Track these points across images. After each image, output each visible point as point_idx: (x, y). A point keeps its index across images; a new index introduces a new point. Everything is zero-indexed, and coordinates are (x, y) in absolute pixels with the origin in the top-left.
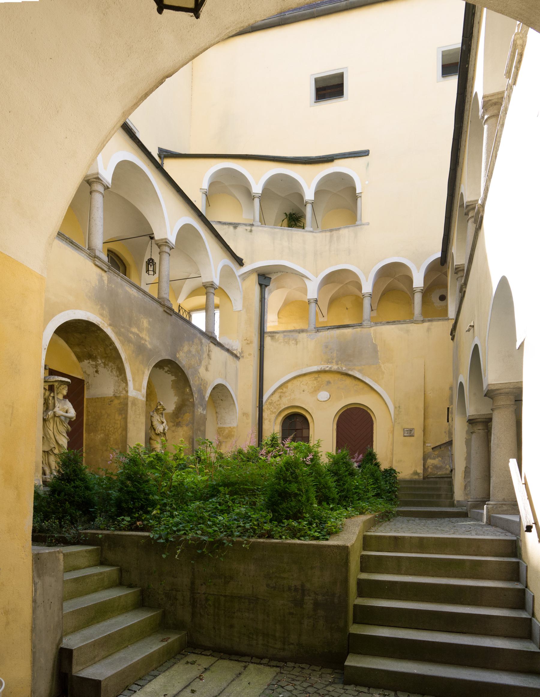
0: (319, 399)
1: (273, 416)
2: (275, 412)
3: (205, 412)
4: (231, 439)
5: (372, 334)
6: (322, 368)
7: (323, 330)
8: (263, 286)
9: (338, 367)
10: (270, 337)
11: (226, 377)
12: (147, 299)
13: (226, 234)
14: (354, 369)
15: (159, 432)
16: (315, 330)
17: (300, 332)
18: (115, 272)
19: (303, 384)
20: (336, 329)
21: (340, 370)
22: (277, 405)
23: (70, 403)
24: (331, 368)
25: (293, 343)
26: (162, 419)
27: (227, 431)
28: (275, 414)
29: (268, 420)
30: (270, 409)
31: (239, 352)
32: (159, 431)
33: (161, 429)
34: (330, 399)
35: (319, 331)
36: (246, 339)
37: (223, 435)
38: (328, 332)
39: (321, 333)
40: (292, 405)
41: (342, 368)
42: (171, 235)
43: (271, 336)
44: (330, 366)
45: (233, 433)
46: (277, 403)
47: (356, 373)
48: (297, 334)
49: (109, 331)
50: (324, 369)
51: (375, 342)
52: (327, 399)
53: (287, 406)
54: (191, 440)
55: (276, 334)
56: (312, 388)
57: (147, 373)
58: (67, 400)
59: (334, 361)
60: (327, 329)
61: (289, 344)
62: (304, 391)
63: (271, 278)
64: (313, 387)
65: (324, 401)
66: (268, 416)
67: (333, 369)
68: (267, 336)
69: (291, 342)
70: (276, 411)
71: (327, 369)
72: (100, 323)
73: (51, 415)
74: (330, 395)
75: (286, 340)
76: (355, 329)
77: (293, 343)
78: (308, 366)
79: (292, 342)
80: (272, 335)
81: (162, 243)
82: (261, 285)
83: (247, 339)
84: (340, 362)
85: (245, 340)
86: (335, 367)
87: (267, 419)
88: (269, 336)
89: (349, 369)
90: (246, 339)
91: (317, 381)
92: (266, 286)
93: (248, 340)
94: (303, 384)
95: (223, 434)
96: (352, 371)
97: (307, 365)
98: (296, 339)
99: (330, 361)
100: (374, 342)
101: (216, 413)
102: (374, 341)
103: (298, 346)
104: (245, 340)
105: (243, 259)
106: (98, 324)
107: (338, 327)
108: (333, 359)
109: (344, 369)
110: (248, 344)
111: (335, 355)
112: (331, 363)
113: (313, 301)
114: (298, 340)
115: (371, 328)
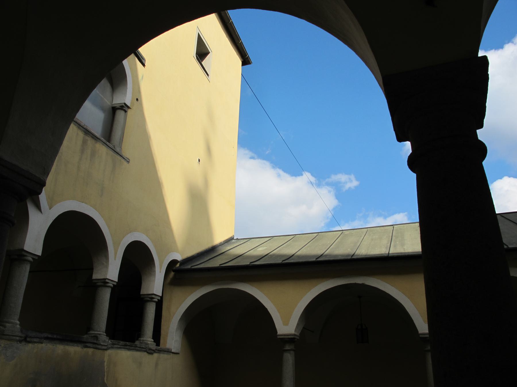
5: (105, 364)
16: (20, 334)
35: (28, 339)
38: (43, 345)
39: (30, 345)
51: (107, 380)
76: (85, 349)
100: (105, 381)
102: (105, 378)
115: (105, 351)
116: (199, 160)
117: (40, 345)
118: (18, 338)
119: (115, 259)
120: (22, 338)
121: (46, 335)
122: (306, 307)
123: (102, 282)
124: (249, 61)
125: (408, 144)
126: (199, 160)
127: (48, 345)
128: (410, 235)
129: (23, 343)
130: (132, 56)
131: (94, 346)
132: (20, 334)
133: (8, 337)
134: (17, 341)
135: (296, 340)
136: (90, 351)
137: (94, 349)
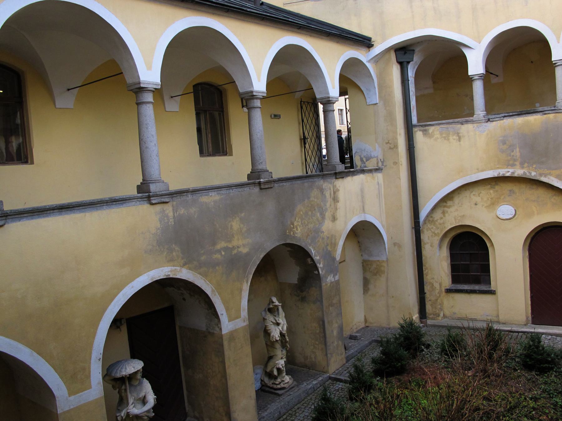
0: (499, 216)
1: (436, 240)
2: (438, 233)
3: (337, 278)
4: (381, 276)
6: (500, 173)
7: (496, 119)
8: (405, 64)
9: (524, 172)
10: (421, 132)
11: (363, 207)
12: (234, 192)
13: (344, 9)
14: (550, 174)
15: (274, 340)
16: (484, 119)
17: (464, 123)
18: (181, 193)
19: (474, 195)
20: (516, 116)
21: (528, 175)
22: (440, 224)
23: (149, 384)
24: (513, 173)
25: (454, 139)
26: (277, 319)
27: (374, 266)
28: (438, 236)
29: (429, 244)
30: (430, 230)
31: (381, 160)
32: (274, 338)
33: (277, 336)
34: (516, 216)
35: (491, 120)
36: (388, 143)
37: (371, 270)
38: (504, 120)
39: (494, 122)
40: (460, 224)
41: (530, 173)
42: (259, 81)
43: (423, 131)
44: (511, 170)
45: (382, 269)
46: (439, 221)
47: (553, 181)
48: (459, 126)
49: (185, 274)
50: (504, 174)
52: (511, 216)
53: (454, 226)
54: (321, 323)
55: (429, 127)
56: (488, 199)
57: (246, 287)
58: (145, 379)
59: (517, 163)
60: (502, 117)
61: (448, 140)
62: (476, 204)
63: (414, 50)
64: (490, 199)
65: (507, 219)
66: (429, 239)
67: (516, 175)
68: (417, 131)
69: (451, 138)
70: (439, 232)
71: (508, 175)
72: (169, 273)
73: (124, 416)
74: (515, 211)
75: (444, 135)
76: (545, 116)
77: (454, 139)
78: (479, 170)
79: (454, 137)
80: (424, 128)
81: (248, 97)
82: (401, 63)
83: (390, 142)
84: (526, 165)
85: (387, 143)
86: (519, 172)
87: (428, 243)
88: (420, 130)
89: (541, 175)
90: (388, 143)
91: (494, 189)
92: (408, 62)
93: (390, 144)
94: (474, 195)
95: (370, 269)
96: (545, 176)
97: (478, 169)
98: (458, 134)
99: (511, 162)
101: (359, 242)
103: (462, 142)
104: (387, 143)
105: (371, 38)
106: (167, 276)
107: (520, 113)
108: (515, 160)
109: (533, 174)
110: (390, 148)
111: (518, 154)
112: (513, 165)
113: (477, 78)
114: (461, 135)
116: (25, 203)
117: (502, 121)
118: (483, 121)
119: (559, 42)
120: (487, 120)
121: (503, 115)
122: (28, 5)
123: (479, 76)
124: (26, 158)
125: (154, 414)
126: (25, 203)
127: (508, 120)
128: (295, 305)
129: (489, 122)
130: (192, 91)
131: (554, 111)
132: (484, 119)
133: (477, 122)
134: (484, 122)
135: (316, 272)
136: (551, 116)
137: (555, 114)
